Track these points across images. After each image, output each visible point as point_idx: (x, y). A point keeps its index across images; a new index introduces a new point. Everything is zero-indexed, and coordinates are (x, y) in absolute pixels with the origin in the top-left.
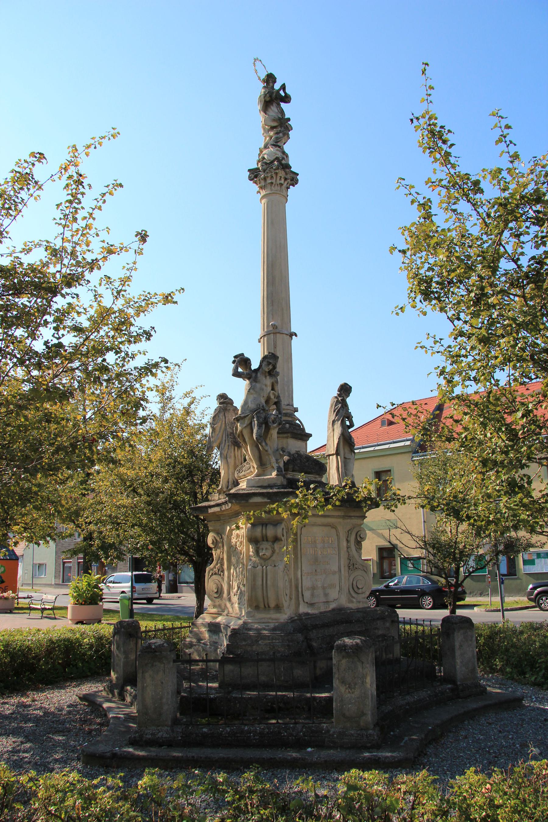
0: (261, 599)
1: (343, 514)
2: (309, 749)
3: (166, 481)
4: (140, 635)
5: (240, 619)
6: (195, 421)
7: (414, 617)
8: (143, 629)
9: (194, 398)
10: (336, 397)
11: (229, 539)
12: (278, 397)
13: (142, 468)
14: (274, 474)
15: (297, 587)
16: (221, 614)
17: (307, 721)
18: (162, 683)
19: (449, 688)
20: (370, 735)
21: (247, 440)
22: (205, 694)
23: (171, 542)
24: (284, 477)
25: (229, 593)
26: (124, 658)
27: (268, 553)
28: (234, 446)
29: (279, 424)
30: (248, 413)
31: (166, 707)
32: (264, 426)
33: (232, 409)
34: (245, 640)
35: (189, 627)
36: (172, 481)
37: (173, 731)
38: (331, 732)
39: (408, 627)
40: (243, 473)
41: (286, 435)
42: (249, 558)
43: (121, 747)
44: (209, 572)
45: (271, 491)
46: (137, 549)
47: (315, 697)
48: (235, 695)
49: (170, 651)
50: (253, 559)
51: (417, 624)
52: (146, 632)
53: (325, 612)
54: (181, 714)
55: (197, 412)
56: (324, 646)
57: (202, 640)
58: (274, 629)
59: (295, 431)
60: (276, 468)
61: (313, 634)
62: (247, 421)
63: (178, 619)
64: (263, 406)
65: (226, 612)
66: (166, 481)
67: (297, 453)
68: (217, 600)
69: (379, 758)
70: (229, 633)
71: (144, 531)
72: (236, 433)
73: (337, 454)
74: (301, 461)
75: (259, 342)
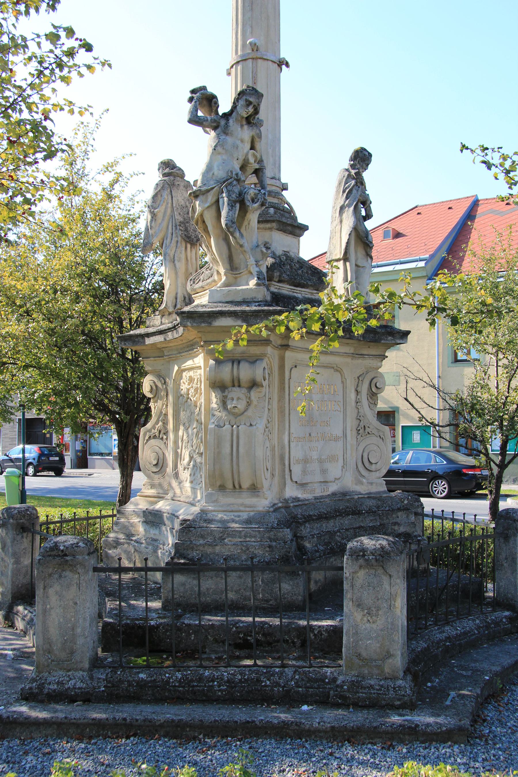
0: (228, 475)
1: (352, 351)
2: (305, 708)
3: (77, 299)
4: (38, 528)
5: (193, 505)
6: (120, 212)
7: (448, 510)
8: (42, 518)
9: (120, 174)
10: (347, 170)
11: (177, 384)
12: (260, 161)
13: (40, 279)
14: (253, 283)
15: (282, 458)
16: (162, 498)
17: (300, 663)
18: (76, 603)
19: (506, 617)
20: (399, 687)
21: (210, 228)
22: (141, 619)
23: (86, 392)
24: (268, 290)
25: (175, 467)
26: (13, 564)
27: (241, 406)
28: (186, 242)
29: (262, 205)
30: (212, 184)
31: (80, 641)
32: (238, 205)
33: (182, 184)
34: (203, 537)
35: (113, 516)
36: (87, 299)
37: (91, 678)
38: (339, 682)
39: (437, 523)
40: (200, 284)
41: (268, 225)
42: (210, 412)
43: (8, 704)
44: (145, 435)
45: (247, 309)
46: (34, 402)
47: (311, 628)
48: (190, 620)
49: (89, 554)
50: (217, 414)
51: (453, 520)
52: (48, 523)
53: (322, 497)
54: (103, 651)
55: (124, 197)
56: (321, 548)
57: (133, 535)
58: (248, 521)
59: (284, 220)
60: (255, 273)
61: (306, 530)
62: (211, 198)
63: (93, 505)
64: (237, 175)
65: (169, 496)
66: (77, 299)
67: (285, 255)
68: (156, 476)
69: (417, 726)
70: (177, 527)
71: (44, 375)
72: (193, 217)
73: (346, 258)
74: (291, 267)
75: (229, 74)
